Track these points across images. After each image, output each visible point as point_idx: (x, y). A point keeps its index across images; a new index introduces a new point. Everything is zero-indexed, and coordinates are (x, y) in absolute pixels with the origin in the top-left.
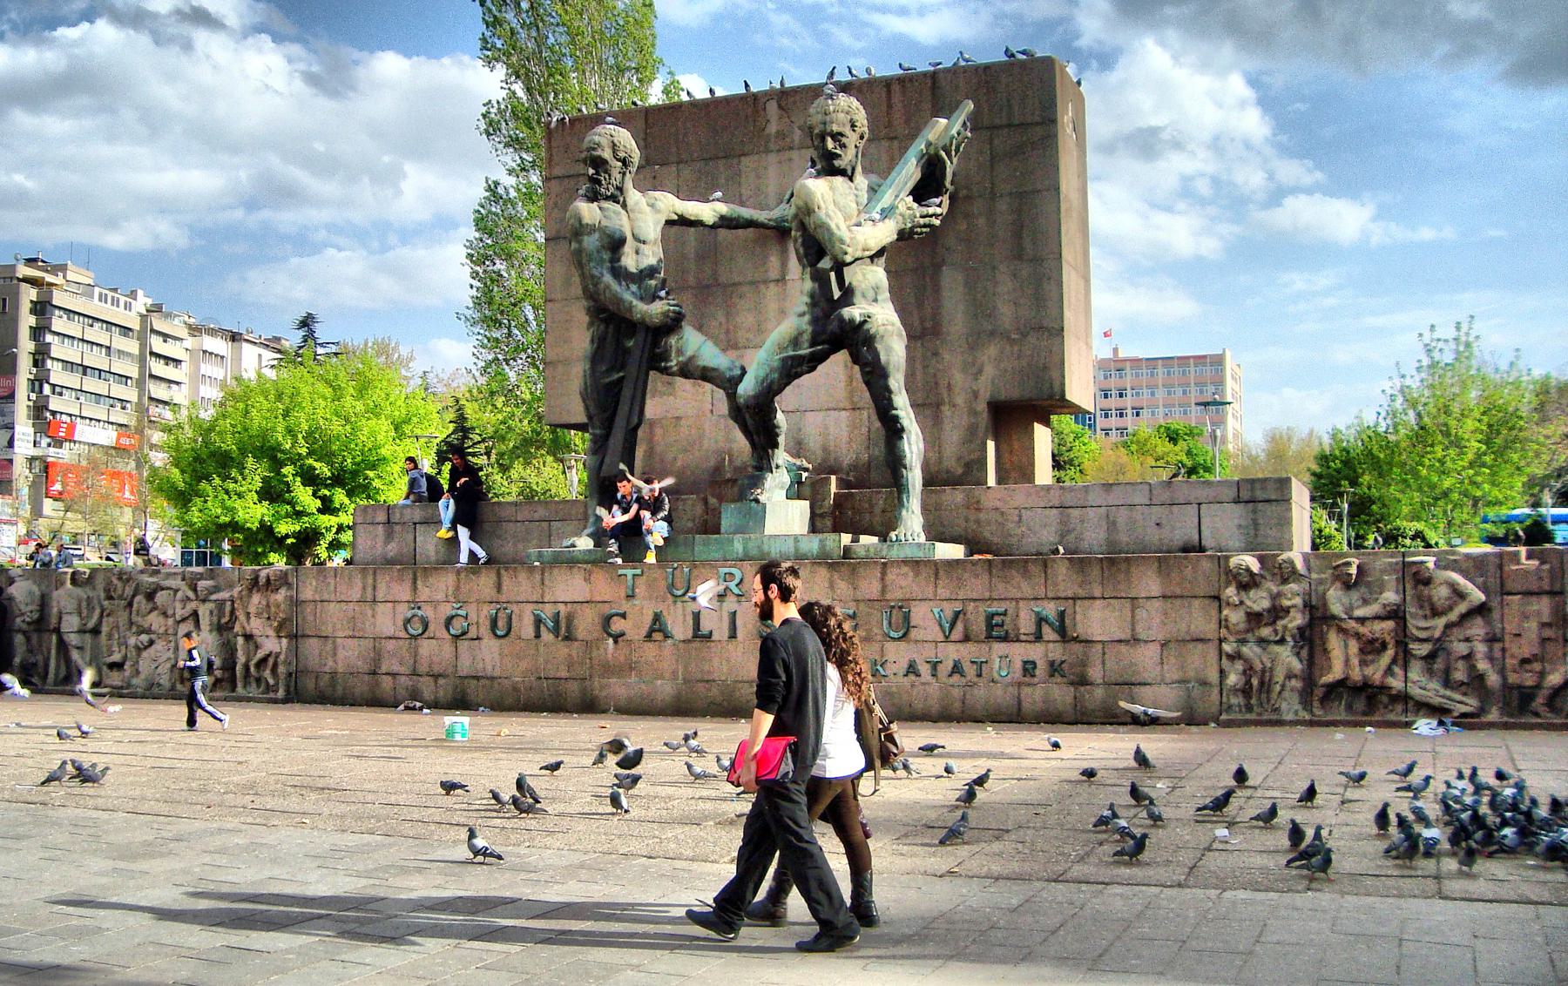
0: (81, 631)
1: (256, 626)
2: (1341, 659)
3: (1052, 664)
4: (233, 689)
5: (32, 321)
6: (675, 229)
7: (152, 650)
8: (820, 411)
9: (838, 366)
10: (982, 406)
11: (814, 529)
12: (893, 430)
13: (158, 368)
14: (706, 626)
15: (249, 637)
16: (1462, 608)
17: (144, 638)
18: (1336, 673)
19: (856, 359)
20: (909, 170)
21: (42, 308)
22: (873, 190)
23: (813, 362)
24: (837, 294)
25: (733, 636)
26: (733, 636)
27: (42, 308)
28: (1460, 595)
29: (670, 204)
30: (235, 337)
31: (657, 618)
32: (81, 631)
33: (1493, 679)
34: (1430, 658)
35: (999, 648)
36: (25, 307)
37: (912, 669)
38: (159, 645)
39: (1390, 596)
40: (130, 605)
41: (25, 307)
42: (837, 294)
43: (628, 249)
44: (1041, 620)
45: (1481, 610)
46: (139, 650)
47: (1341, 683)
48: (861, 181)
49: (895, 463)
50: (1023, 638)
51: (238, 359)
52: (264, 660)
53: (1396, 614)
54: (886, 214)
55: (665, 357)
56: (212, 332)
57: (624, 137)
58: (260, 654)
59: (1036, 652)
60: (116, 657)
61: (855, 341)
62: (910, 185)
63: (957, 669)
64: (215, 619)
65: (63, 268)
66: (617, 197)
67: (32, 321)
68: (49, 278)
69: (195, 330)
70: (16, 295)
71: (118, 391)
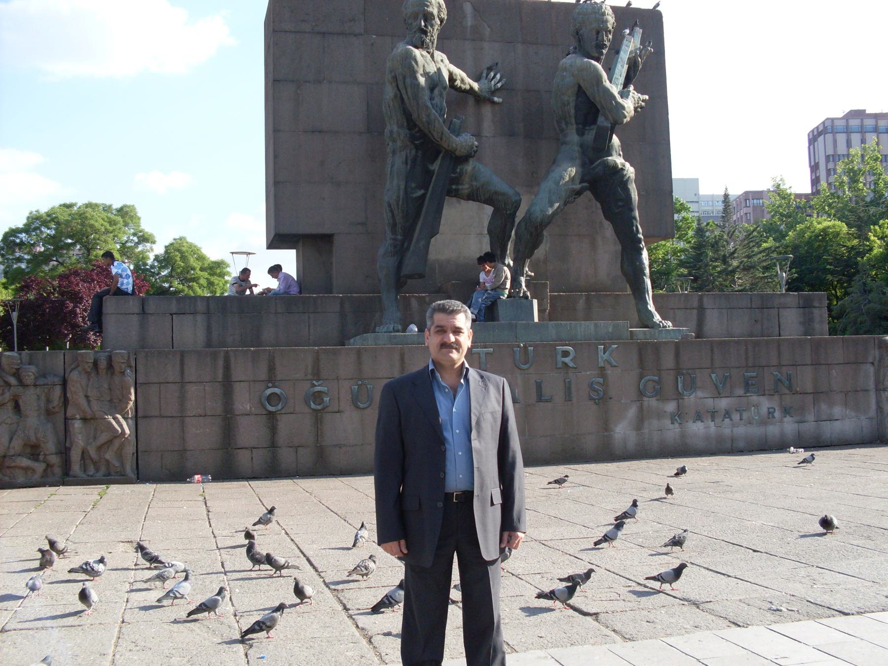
14: (547, 391)
26: (568, 397)
52: (110, 442)
55: (457, 181)
58: (104, 438)
64: (42, 404)
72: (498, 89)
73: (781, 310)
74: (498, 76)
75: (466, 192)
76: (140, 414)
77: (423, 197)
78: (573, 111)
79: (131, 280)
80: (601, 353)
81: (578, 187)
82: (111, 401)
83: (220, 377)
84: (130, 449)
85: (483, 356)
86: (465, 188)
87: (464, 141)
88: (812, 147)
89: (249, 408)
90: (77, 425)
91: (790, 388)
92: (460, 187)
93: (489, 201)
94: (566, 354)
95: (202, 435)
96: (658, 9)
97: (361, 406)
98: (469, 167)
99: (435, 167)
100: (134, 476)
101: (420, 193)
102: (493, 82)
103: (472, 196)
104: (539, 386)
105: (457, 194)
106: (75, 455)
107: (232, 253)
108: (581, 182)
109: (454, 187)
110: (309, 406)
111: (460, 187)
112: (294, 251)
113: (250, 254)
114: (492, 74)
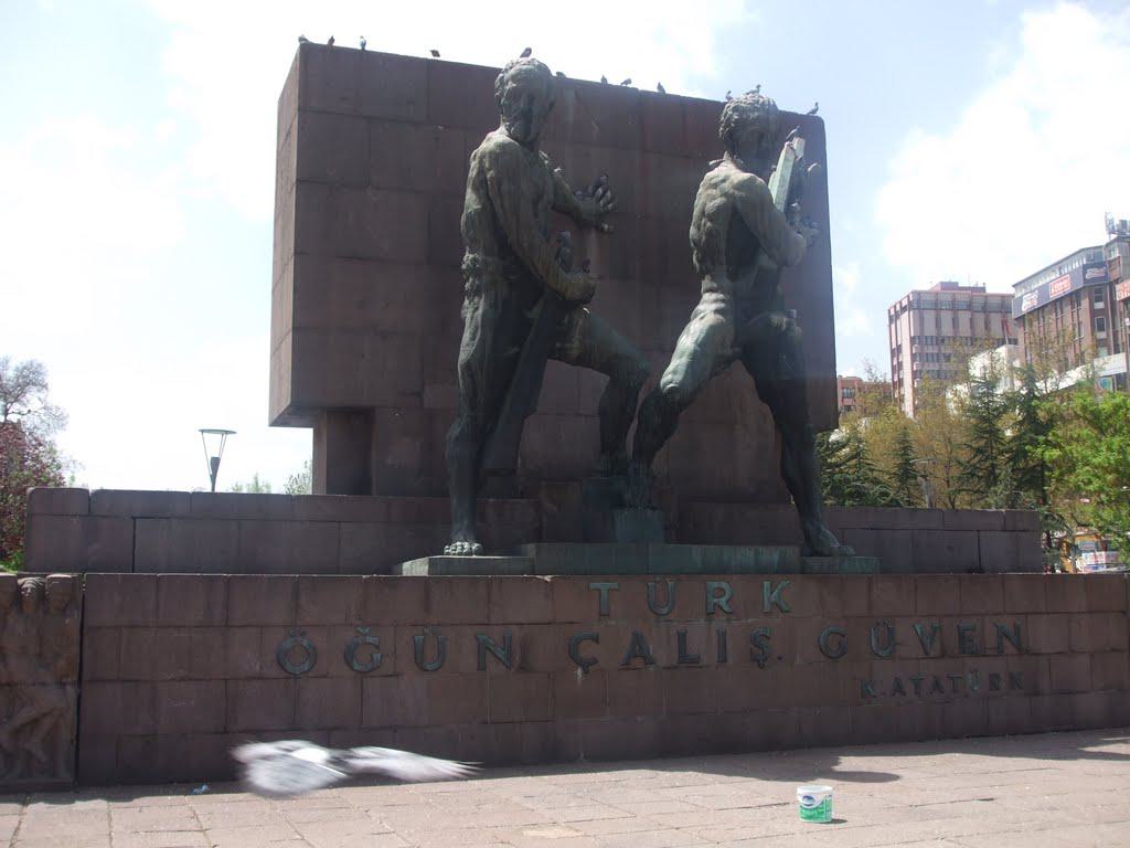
3: (1011, 676)
25: (723, 660)
31: (638, 640)
37: (899, 688)
44: (1002, 634)
63: (937, 685)
72: (608, 212)
73: (982, 534)
74: (609, 194)
75: (575, 353)
76: (86, 676)
77: (518, 354)
78: (723, 246)
79: (959, 387)
80: (766, 592)
81: (729, 352)
82: (40, 655)
84: (66, 735)
85: (604, 592)
86: (575, 346)
87: (573, 282)
88: (893, 326)
89: (258, 667)
92: (568, 345)
93: (603, 369)
94: (721, 592)
96: (818, 114)
97: (428, 667)
99: (534, 313)
100: (65, 775)
101: (516, 349)
102: (601, 202)
103: (583, 360)
104: (682, 637)
105: (562, 356)
107: (203, 431)
108: (732, 347)
109: (558, 345)
110: (351, 667)
111: (568, 345)
112: (311, 430)
113: (227, 432)
114: (600, 190)
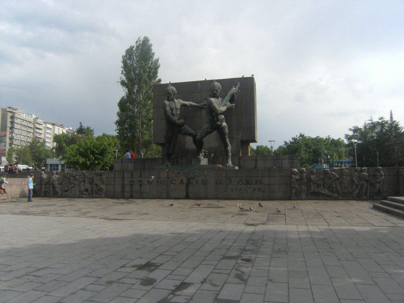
0: (59, 184)
1: (98, 183)
2: (313, 188)
4: (93, 195)
5: (10, 120)
6: (183, 107)
7: (74, 188)
8: (211, 141)
9: (215, 133)
10: (239, 141)
11: (209, 164)
12: (226, 146)
13: (37, 131)
15: (96, 185)
16: (335, 178)
17: (73, 185)
18: (313, 190)
19: (219, 132)
20: (228, 97)
21: (12, 117)
22: (222, 101)
23: (210, 132)
24: (216, 120)
27: (12, 117)
28: (335, 176)
29: (181, 101)
30: (53, 125)
31: (182, 180)
32: (59, 184)
33: (340, 191)
34: (329, 187)
35: (249, 186)
36: (9, 117)
38: (76, 187)
39: (322, 176)
40: (69, 179)
41: (9, 117)
42: (216, 120)
43: (174, 110)
45: (338, 179)
46: (72, 187)
47: (313, 192)
48: (220, 99)
49: (226, 151)
50: (171, 296)
51: (54, 129)
52: (100, 190)
53: (323, 179)
54: (225, 105)
56: (49, 123)
57: (174, 88)
58: (99, 188)
59: (256, 187)
60: (66, 189)
61: (220, 129)
62: (228, 100)
63: (241, 190)
65: (17, 109)
66: (173, 100)
67: (10, 120)
68: (14, 111)
69: (45, 123)
70: (7, 115)
71: (29, 135)
83: (122, 176)
90: (95, 185)
91: (261, 183)
94: (197, 172)
95: (118, 188)
98: (183, 128)
106: (94, 192)
